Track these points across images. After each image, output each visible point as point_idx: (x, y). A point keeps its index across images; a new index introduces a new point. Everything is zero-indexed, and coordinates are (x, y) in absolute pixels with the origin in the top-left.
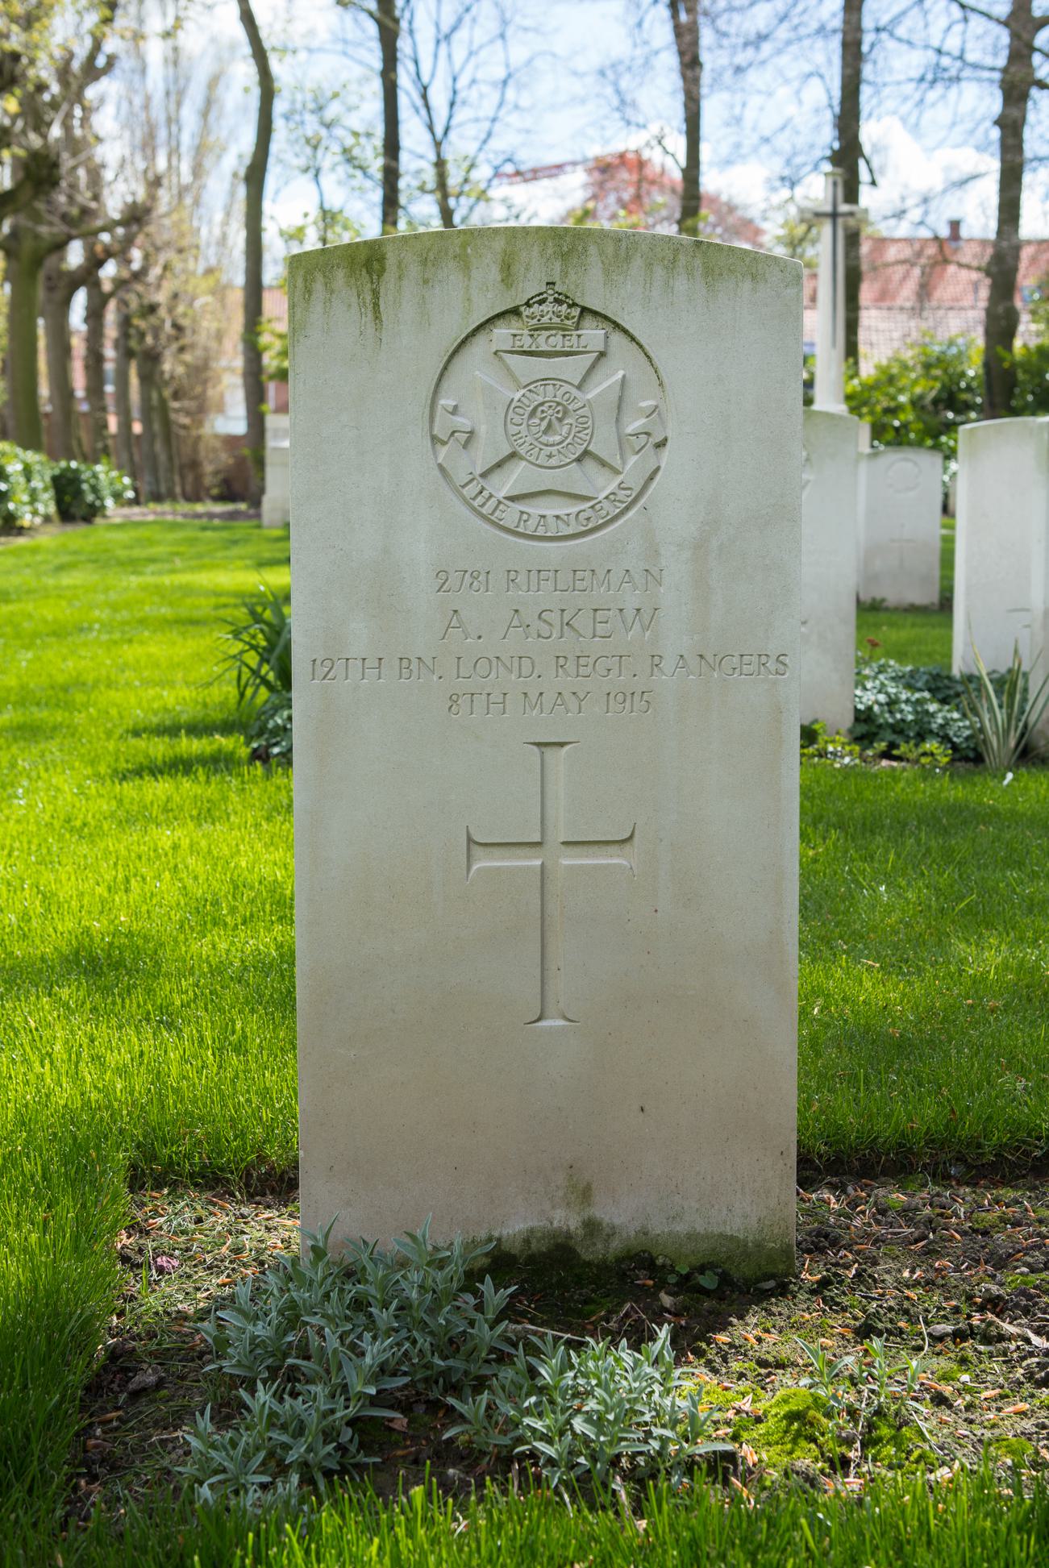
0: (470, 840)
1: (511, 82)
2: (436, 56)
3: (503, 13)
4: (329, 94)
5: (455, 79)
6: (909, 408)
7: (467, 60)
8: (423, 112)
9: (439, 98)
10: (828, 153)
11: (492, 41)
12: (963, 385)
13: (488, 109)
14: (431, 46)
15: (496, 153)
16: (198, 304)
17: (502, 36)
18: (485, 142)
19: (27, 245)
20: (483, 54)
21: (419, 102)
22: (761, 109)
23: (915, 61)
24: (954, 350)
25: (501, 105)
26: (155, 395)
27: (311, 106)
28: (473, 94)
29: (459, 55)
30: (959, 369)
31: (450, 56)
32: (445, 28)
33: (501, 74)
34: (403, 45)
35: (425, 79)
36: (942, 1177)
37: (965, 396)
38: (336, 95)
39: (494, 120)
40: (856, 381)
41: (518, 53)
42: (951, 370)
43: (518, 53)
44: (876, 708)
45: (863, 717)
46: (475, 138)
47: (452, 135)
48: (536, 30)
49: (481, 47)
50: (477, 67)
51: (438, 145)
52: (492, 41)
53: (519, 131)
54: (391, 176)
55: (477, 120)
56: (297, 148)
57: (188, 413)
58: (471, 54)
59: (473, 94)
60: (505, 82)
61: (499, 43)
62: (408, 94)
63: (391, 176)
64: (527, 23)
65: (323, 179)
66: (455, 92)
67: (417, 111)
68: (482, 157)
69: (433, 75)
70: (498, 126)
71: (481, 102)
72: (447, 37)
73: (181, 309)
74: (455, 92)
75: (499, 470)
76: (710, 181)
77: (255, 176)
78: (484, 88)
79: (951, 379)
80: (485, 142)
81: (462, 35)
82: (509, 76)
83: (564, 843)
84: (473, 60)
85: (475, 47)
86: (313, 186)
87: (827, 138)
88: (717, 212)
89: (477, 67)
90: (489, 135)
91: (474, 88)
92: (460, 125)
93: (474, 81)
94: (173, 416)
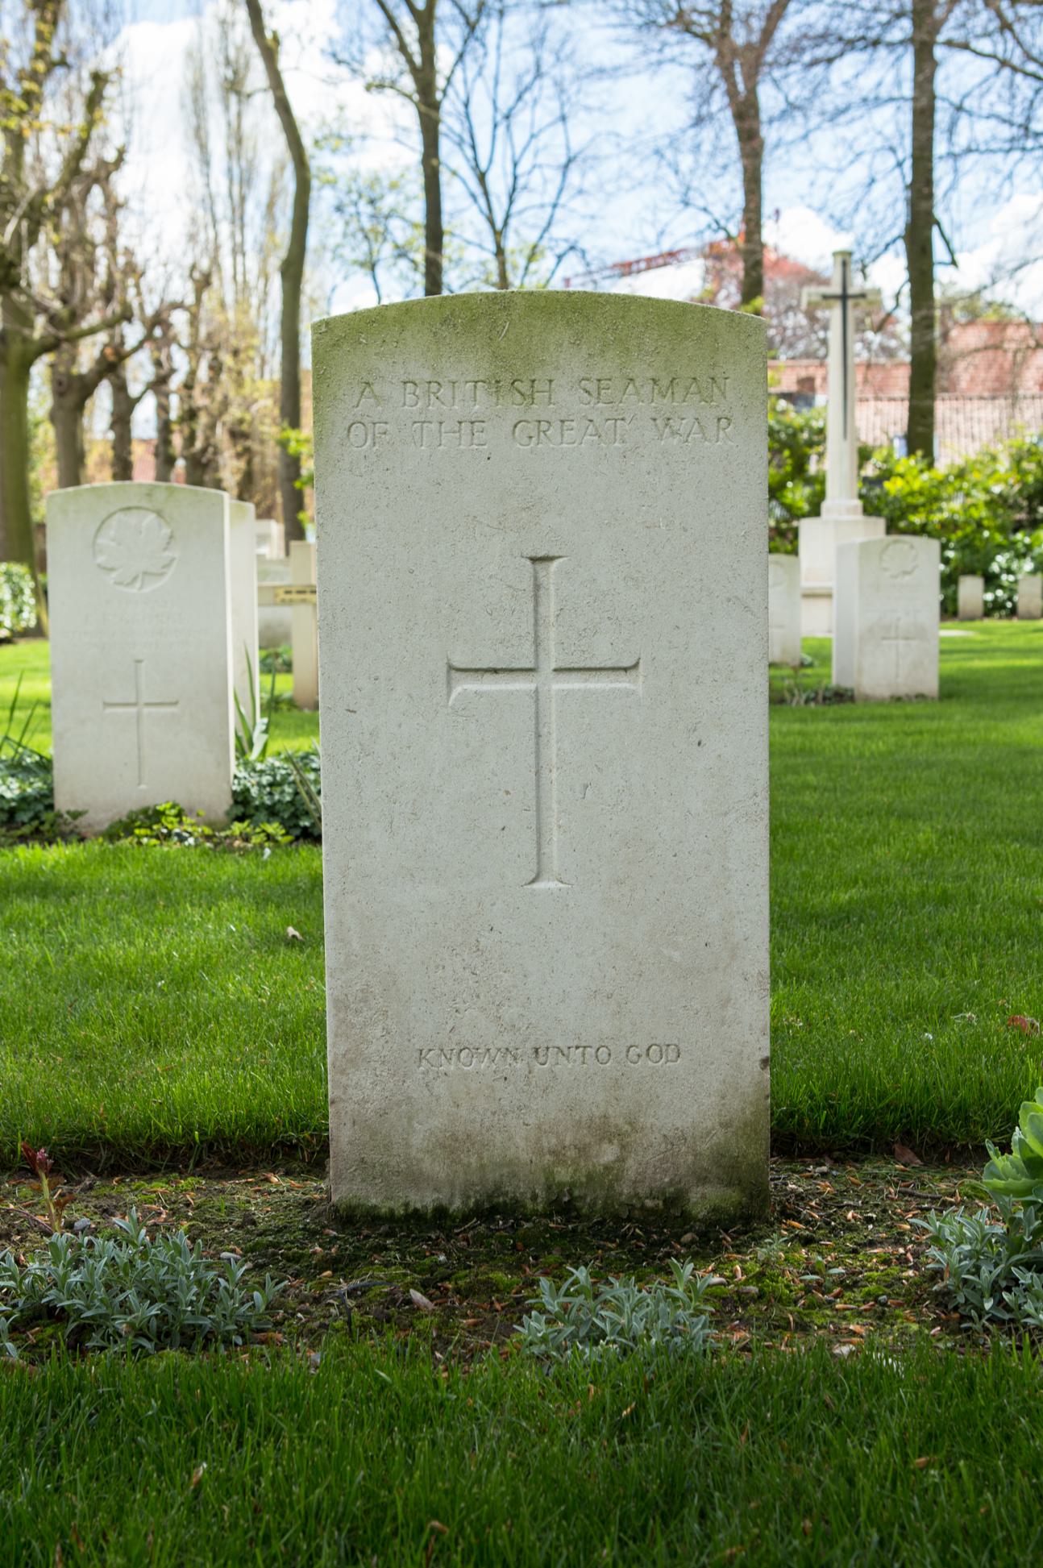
1: (572, 166)
2: (494, 138)
4: (386, 183)
5: (515, 165)
8: (482, 201)
16: (254, 408)
17: (563, 118)
18: (546, 229)
20: (543, 139)
25: (561, 191)
28: (536, 179)
29: (520, 136)
32: (503, 108)
33: (563, 160)
35: (483, 165)
39: (555, 206)
40: (926, 476)
41: (580, 133)
44: (254, 791)
45: (240, 799)
47: (513, 222)
48: (600, 109)
49: (541, 131)
50: (536, 154)
51: (498, 235)
53: (584, 217)
55: (542, 206)
56: (350, 240)
58: (533, 136)
59: (536, 179)
60: (566, 167)
61: (560, 126)
64: (592, 101)
67: (474, 197)
69: (491, 161)
71: (541, 185)
72: (507, 117)
74: (515, 178)
75: (541, 592)
77: (293, 271)
80: (546, 229)
81: (522, 118)
82: (570, 161)
86: (369, 279)
88: (165, 334)
89: (536, 154)
90: (549, 224)
92: (521, 212)
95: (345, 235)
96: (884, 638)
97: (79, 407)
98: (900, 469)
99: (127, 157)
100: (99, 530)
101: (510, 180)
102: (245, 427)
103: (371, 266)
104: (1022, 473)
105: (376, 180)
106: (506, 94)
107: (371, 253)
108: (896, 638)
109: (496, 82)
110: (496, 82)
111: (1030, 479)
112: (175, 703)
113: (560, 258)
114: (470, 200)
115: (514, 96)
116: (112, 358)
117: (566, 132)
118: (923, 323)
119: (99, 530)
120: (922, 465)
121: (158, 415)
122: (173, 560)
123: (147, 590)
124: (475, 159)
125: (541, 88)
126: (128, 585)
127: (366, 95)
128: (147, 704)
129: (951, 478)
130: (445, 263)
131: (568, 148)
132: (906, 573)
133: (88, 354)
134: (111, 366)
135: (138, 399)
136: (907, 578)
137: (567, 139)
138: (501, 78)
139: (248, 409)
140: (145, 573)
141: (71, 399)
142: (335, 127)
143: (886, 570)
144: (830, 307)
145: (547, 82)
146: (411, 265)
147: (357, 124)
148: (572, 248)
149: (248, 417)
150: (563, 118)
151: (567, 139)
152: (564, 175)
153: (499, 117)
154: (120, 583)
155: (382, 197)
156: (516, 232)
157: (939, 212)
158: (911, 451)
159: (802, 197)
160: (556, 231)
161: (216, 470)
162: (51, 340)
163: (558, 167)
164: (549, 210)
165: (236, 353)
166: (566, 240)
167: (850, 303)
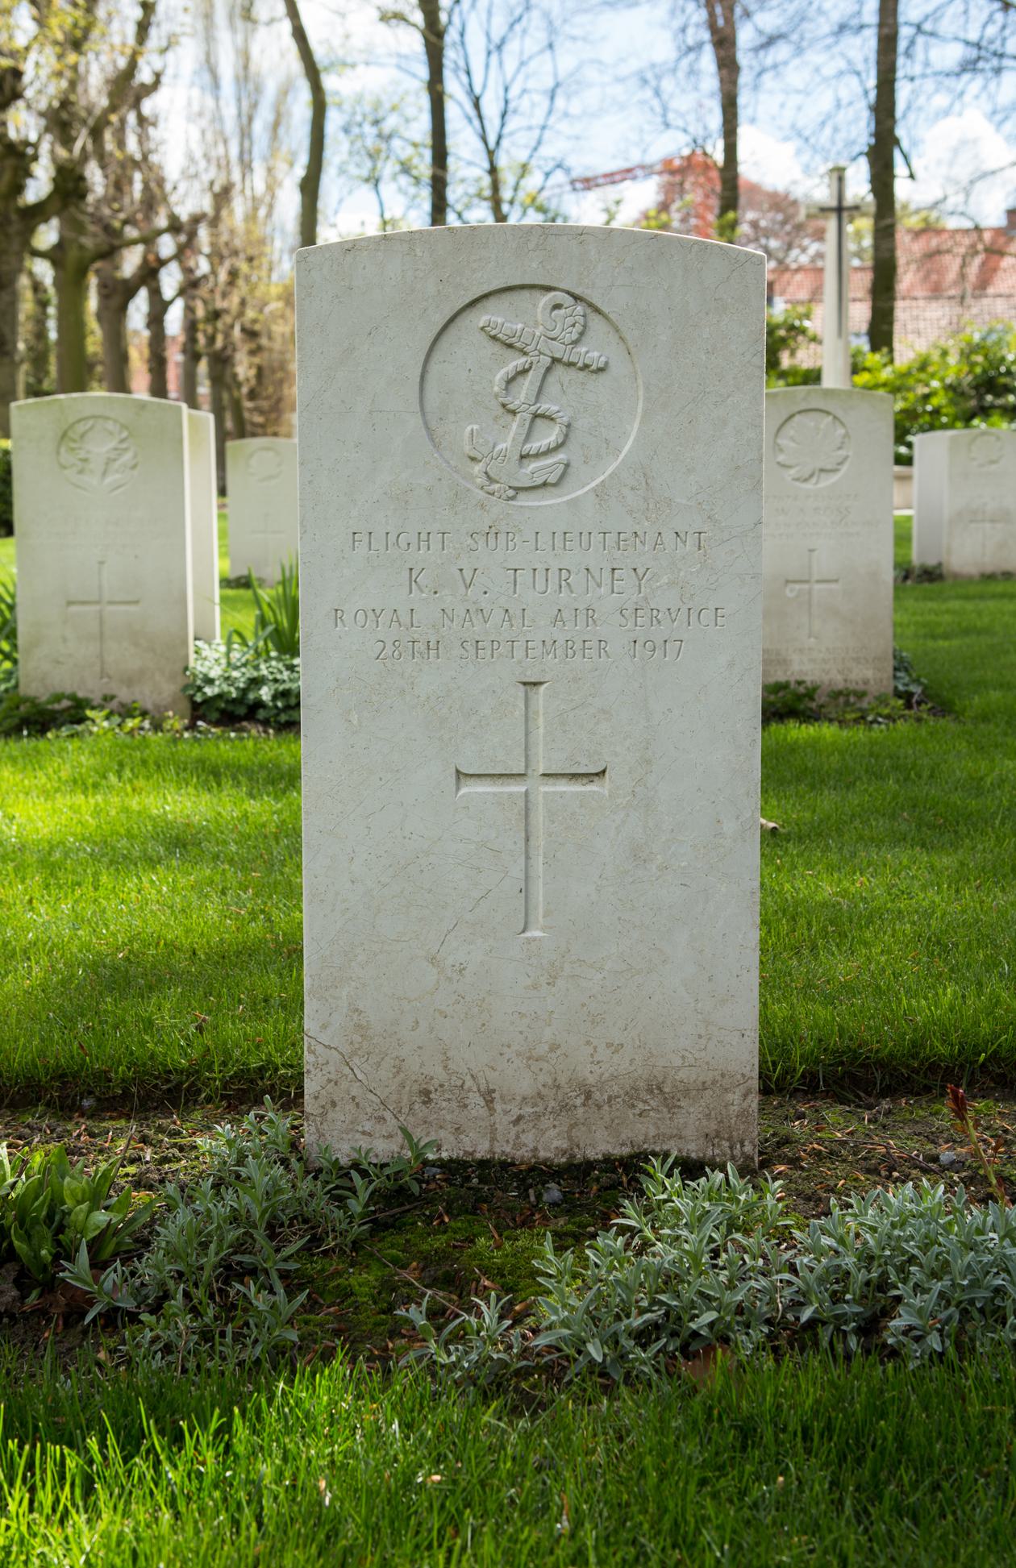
0: (458, 771)
1: (559, 91)
2: (487, 66)
3: (550, 23)
4: (387, 106)
5: (506, 89)
6: (942, 393)
7: (518, 71)
8: (476, 122)
9: (491, 108)
10: (866, 149)
11: (542, 51)
12: (1003, 369)
13: (538, 118)
14: (483, 56)
15: (546, 159)
16: (267, 310)
17: (551, 46)
19: (73, 254)
20: (533, 65)
21: (472, 113)
22: (799, 108)
23: (950, 54)
24: (994, 337)
25: (550, 112)
26: (225, 396)
27: (370, 118)
28: (525, 103)
29: (511, 65)
30: (999, 355)
31: (501, 64)
32: (496, 39)
33: (550, 84)
34: (450, 56)
35: (477, 90)
36: (881, 25)
37: (1003, 380)
38: (393, 109)
39: (543, 128)
40: (889, 369)
41: (566, 61)
42: (991, 355)
43: (566, 61)
46: (526, 147)
47: (505, 143)
48: (585, 39)
49: (530, 58)
50: (527, 77)
51: (491, 154)
52: (542, 51)
54: (439, 185)
55: (530, 128)
56: (357, 158)
57: (261, 412)
58: (522, 64)
59: (525, 103)
61: (548, 54)
62: (460, 104)
63: (439, 185)
64: (576, 32)
65: (381, 186)
66: (506, 102)
67: (470, 120)
68: (533, 162)
69: (484, 86)
70: (547, 134)
71: (530, 110)
72: (499, 48)
73: (250, 314)
74: (506, 102)
76: (747, 170)
77: (310, 187)
78: (537, 98)
79: (990, 363)
80: (535, 149)
81: (512, 47)
82: (557, 85)
83: (544, 775)
84: (524, 70)
85: (525, 57)
86: (373, 195)
87: (861, 131)
90: (539, 142)
91: (526, 97)
92: (511, 134)
93: (524, 91)
94: (246, 415)
95: (351, 153)
96: (972, 521)
97: (123, 309)
98: (868, 364)
99: (164, 80)
100: (779, 430)
101: (502, 104)
102: (257, 327)
103: (374, 181)
104: (972, 365)
105: (378, 105)
106: (499, 27)
107: (374, 169)
108: (983, 521)
109: (489, 13)
110: (489, 13)
111: (978, 370)
112: (836, 581)
113: (547, 175)
114: (465, 122)
115: (506, 28)
116: (154, 265)
117: (554, 59)
118: (885, 232)
119: (779, 430)
120: (885, 360)
121: (185, 316)
122: (846, 458)
123: (821, 485)
124: (470, 85)
125: (529, 20)
126: (806, 480)
127: (382, 26)
128: (818, 581)
129: (914, 372)
130: (449, 179)
131: (555, 75)
132: (993, 462)
133: (131, 262)
134: (149, 274)
135: (171, 302)
136: (993, 467)
137: (555, 67)
138: (494, 10)
139: (261, 311)
140: (822, 470)
141: (115, 301)
142: (341, 53)
143: (974, 459)
144: (826, 218)
145: (535, 14)
146: (412, 180)
147: (361, 51)
148: (559, 166)
149: (261, 317)
150: (551, 46)
151: (555, 67)
152: (552, 98)
153: (492, 47)
154: (797, 480)
155: (384, 119)
156: (508, 152)
157: (900, 132)
158: (875, 348)
159: (774, 118)
160: (544, 151)
161: (233, 365)
162: (105, 248)
163: (545, 92)
164: (537, 132)
165: (250, 259)
166: (553, 159)
167: (845, 215)
